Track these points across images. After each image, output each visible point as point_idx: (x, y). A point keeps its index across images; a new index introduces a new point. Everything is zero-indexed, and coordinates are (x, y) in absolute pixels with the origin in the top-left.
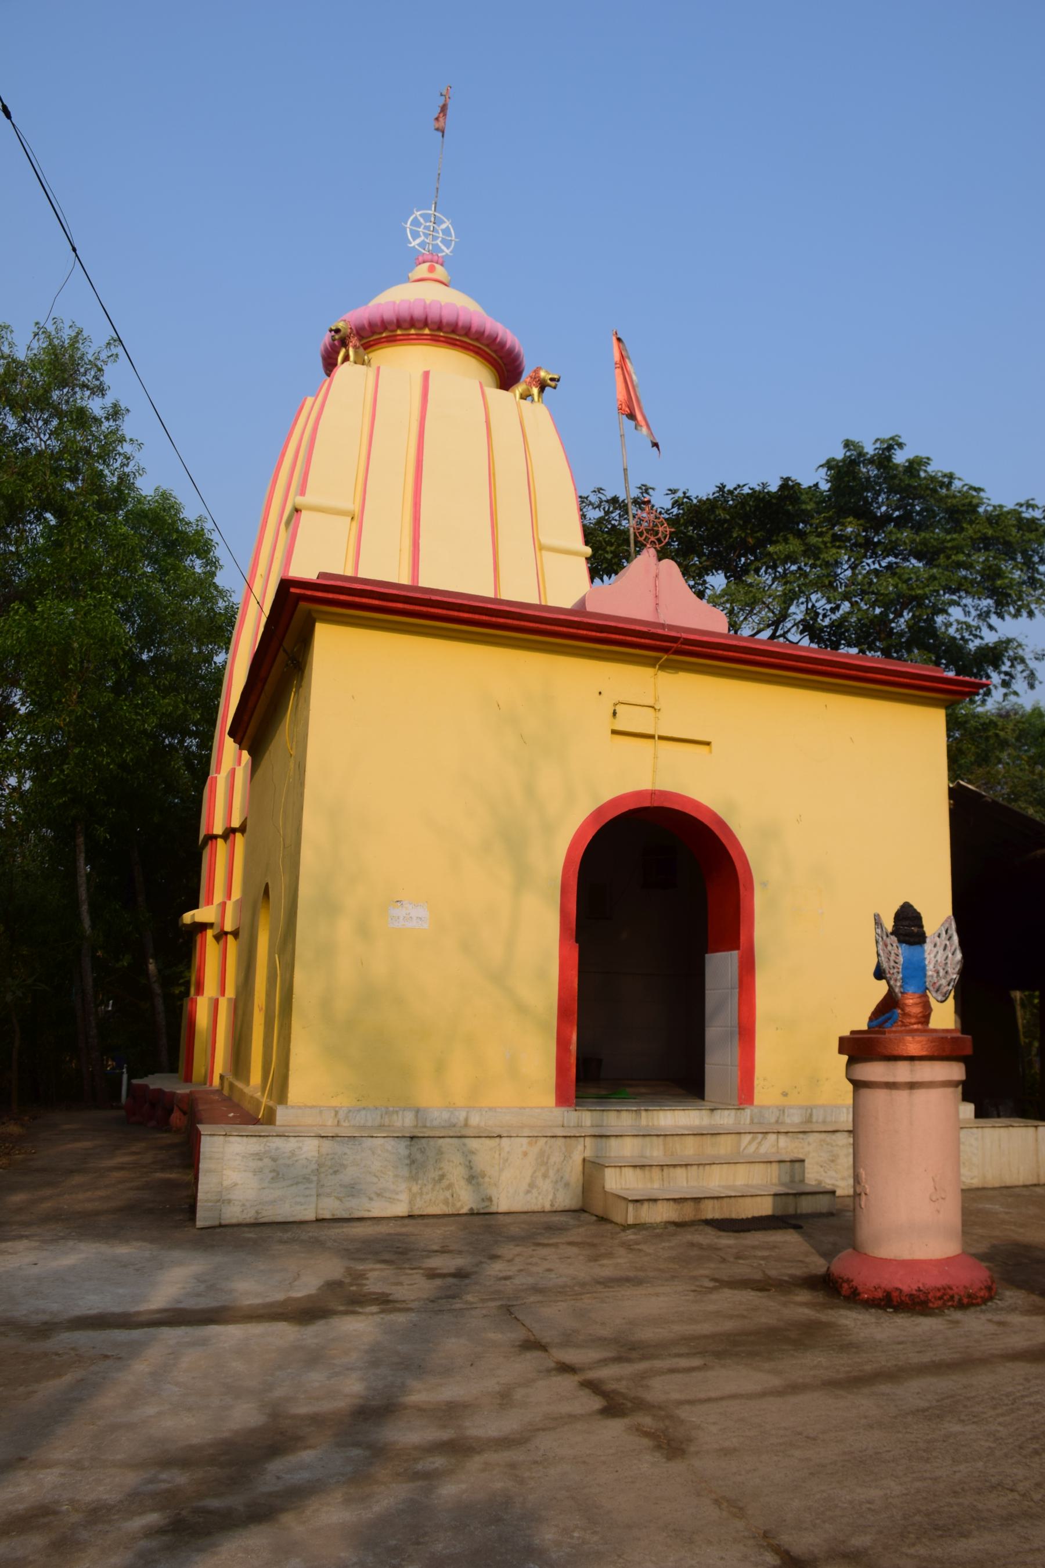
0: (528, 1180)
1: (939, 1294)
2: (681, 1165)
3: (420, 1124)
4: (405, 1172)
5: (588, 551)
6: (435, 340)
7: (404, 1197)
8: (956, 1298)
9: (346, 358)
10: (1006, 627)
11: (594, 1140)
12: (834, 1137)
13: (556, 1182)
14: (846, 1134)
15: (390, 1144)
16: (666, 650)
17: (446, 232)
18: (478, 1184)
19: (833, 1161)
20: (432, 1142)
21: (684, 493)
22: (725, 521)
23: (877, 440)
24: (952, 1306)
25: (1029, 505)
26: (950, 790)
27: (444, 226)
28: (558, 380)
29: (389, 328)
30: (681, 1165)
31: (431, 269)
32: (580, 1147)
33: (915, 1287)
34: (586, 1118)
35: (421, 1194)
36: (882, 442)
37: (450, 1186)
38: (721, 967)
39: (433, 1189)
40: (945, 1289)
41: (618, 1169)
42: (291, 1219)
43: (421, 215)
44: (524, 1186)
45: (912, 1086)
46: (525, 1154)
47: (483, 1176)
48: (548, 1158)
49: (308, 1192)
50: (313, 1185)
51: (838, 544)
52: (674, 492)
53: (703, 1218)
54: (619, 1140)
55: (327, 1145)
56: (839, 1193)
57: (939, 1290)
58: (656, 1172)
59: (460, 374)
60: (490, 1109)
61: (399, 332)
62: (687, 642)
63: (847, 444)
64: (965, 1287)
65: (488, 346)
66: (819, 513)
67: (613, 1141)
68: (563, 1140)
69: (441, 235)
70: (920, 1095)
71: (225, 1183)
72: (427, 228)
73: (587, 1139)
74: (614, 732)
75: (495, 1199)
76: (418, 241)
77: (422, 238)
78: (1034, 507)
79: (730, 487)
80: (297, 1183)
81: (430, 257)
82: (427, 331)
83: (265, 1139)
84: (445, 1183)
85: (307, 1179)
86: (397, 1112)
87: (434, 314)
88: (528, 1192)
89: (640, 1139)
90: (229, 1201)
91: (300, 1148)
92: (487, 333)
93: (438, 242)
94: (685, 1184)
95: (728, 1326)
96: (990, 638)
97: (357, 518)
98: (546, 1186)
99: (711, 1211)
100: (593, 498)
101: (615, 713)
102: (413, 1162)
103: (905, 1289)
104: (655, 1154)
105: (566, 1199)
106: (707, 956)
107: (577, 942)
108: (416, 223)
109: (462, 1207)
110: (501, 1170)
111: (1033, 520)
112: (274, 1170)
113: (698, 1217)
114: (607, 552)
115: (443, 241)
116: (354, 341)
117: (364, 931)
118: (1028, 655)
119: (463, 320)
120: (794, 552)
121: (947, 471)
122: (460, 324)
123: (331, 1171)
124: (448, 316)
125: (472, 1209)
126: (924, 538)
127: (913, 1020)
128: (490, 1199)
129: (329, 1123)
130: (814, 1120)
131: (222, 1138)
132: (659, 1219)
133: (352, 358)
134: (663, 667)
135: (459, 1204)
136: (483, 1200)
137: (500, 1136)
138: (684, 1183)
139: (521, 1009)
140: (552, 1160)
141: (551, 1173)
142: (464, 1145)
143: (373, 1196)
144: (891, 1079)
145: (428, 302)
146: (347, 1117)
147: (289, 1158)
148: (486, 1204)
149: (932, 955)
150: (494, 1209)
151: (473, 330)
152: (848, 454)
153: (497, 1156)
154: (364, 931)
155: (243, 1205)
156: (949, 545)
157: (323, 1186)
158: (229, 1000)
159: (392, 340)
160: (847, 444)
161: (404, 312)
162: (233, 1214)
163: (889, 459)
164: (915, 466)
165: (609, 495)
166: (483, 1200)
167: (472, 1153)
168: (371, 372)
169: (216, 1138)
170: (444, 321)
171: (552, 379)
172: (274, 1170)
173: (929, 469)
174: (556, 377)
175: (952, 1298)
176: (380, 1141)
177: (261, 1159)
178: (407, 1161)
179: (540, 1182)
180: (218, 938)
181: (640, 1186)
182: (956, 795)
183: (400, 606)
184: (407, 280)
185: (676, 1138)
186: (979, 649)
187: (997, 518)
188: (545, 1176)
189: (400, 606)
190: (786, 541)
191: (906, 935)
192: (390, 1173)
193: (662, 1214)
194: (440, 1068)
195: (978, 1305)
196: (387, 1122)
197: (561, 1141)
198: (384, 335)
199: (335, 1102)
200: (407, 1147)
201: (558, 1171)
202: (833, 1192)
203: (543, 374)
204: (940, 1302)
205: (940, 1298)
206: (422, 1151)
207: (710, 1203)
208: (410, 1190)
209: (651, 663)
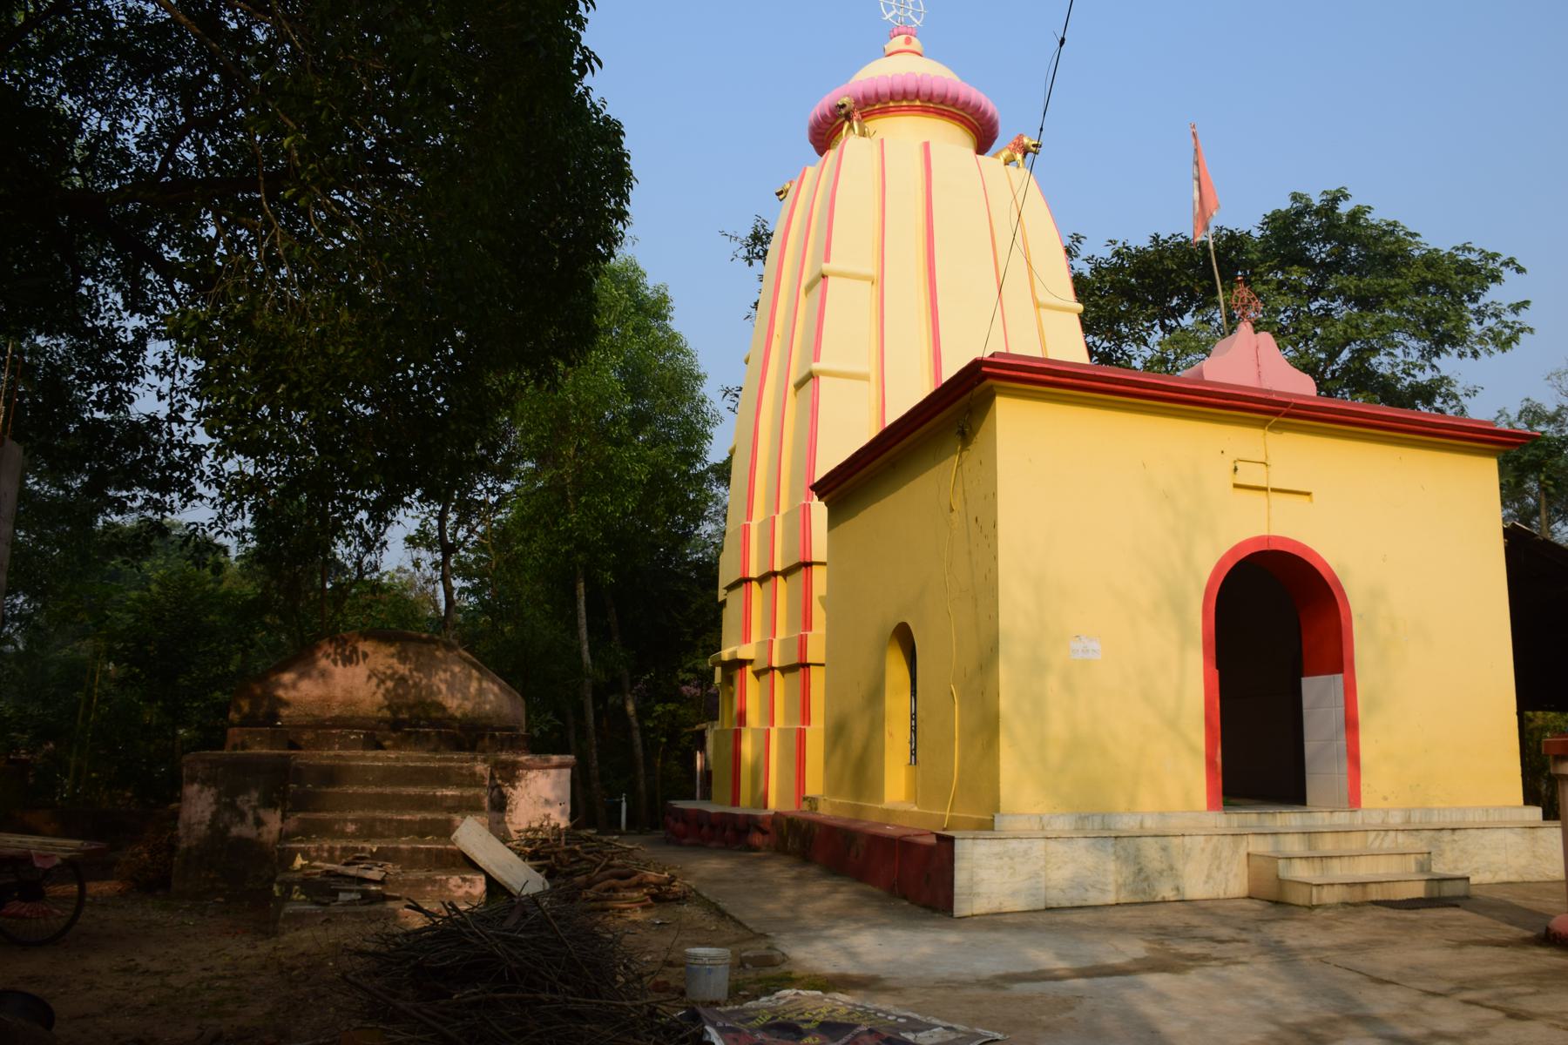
5: (1080, 307)
6: (925, 111)
10: (1449, 364)
16: (1276, 414)
22: (1172, 271)
25: (1466, 248)
26: (1505, 530)
31: (908, 41)
38: (1317, 691)
52: (1113, 242)
56: (1472, 881)
59: (950, 140)
62: (1297, 406)
63: (1295, 197)
74: (1236, 486)
78: (1470, 250)
79: (1164, 236)
84: (1143, 875)
87: (925, 88)
90: (978, 894)
96: (1423, 377)
97: (880, 282)
99: (1375, 894)
106: (1304, 680)
111: (1468, 262)
115: (914, 13)
116: (857, 115)
118: (1459, 391)
121: (1390, 220)
124: (938, 88)
134: (1272, 428)
158: (780, 730)
159: (884, 112)
160: (1295, 197)
161: (899, 87)
163: (1333, 209)
164: (1354, 216)
173: (1368, 216)
180: (758, 674)
182: (1510, 534)
183: (1069, 381)
187: (1432, 261)
189: (1069, 381)
193: (1330, 896)
197: (1229, 839)
202: (1468, 879)
203: (1026, 141)
209: (1262, 425)
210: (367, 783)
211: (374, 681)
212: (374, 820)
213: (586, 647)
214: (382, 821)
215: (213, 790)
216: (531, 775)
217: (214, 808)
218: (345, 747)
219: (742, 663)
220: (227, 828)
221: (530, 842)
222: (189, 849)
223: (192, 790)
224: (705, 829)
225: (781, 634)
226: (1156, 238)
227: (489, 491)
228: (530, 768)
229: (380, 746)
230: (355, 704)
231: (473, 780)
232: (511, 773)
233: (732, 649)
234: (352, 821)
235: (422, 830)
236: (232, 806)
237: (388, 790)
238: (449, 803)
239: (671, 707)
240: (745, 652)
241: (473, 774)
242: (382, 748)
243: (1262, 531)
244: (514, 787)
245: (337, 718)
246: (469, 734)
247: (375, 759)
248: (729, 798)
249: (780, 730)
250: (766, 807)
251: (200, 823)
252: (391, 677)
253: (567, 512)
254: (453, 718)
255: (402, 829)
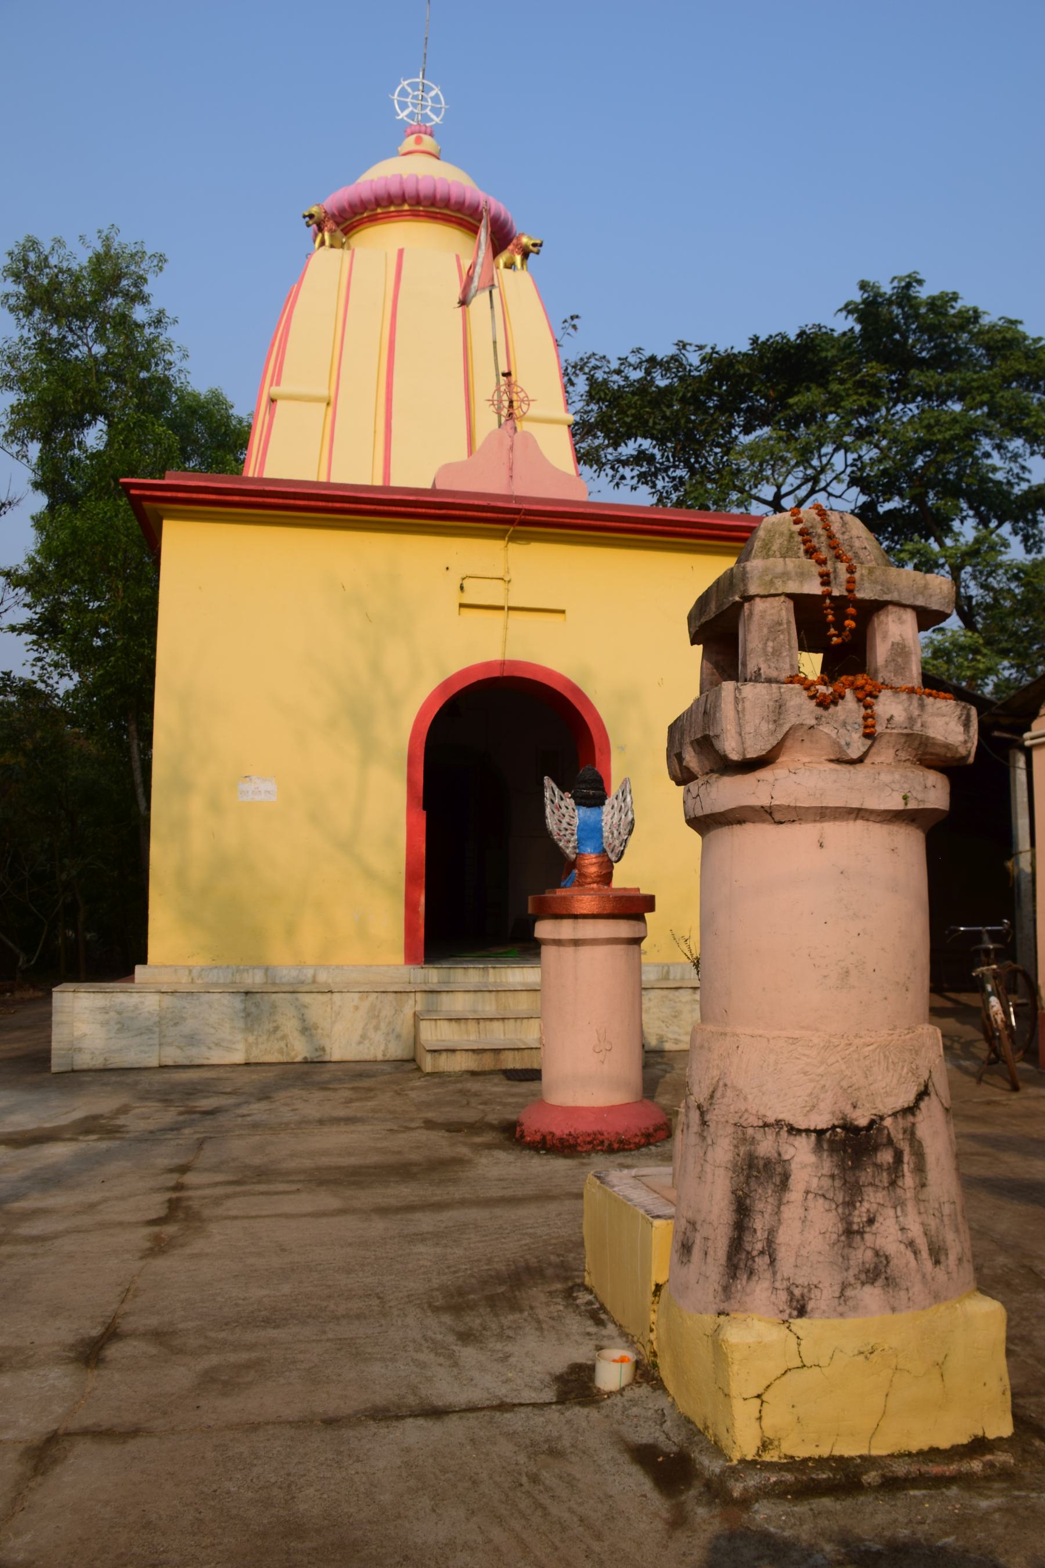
0: (360, 1032)
1: (589, 1139)
2: (498, 1019)
3: (270, 981)
4: (241, 1024)
6: (415, 215)
7: (241, 1046)
8: (606, 1143)
9: (323, 243)
11: (424, 995)
12: (677, 993)
13: (388, 1034)
14: (690, 990)
15: (226, 999)
16: (511, 522)
17: (436, 99)
18: (311, 1035)
19: (675, 1017)
20: (266, 997)
21: (713, 348)
22: (745, 375)
23: (894, 278)
24: (602, 1150)
27: (432, 94)
28: (541, 245)
29: (384, 203)
30: (498, 1019)
31: (418, 141)
32: (411, 1002)
33: (567, 1132)
34: (433, 975)
35: (257, 1044)
36: (901, 279)
37: (284, 1037)
39: (268, 1040)
40: (595, 1134)
41: (433, 1022)
42: (137, 1066)
43: (408, 85)
44: (356, 1037)
45: (576, 943)
46: (357, 1008)
47: (316, 1029)
48: (380, 1012)
49: (151, 1042)
50: (156, 1036)
51: (860, 391)
53: (504, 1068)
54: (450, 995)
55: (168, 1000)
57: (589, 1135)
58: (472, 1026)
60: (337, 967)
61: (379, 211)
63: (863, 286)
64: (617, 1133)
65: (471, 215)
66: (842, 360)
67: (444, 996)
68: (394, 995)
69: (430, 103)
70: (585, 951)
71: (76, 1034)
72: (415, 97)
73: (418, 994)
74: (462, 606)
75: (328, 1049)
76: (406, 112)
77: (411, 109)
80: (141, 1034)
81: (417, 128)
82: (406, 207)
83: (111, 995)
84: (279, 1034)
85: (149, 1030)
86: (247, 970)
87: (410, 189)
88: (360, 1043)
89: (471, 995)
90: (80, 1050)
91: (142, 1003)
92: (467, 204)
93: (428, 111)
94: (502, 1037)
95: (352, 1161)
98: (378, 1037)
100: (633, 359)
101: (462, 588)
102: (248, 1015)
103: (558, 1133)
104: (487, 1008)
105: (397, 1051)
107: (424, 809)
108: (404, 93)
109: (296, 1056)
110: (333, 1023)
112: (119, 1023)
113: (498, 1067)
114: (628, 416)
115: (433, 110)
117: (215, 806)
119: (441, 191)
120: (813, 401)
122: (438, 196)
123: (172, 1023)
124: (425, 189)
125: (305, 1058)
126: (950, 379)
127: (589, 880)
128: (323, 1049)
129: (184, 981)
130: (671, 977)
131: (71, 994)
132: (457, 1068)
133: (327, 243)
134: (513, 539)
135: (293, 1054)
136: (316, 1050)
137: (331, 992)
138: (498, 1035)
139: (370, 874)
140: (383, 1013)
141: (383, 1026)
142: (297, 999)
143: (211, 1045)
144: (557, 937)
145: (405, 177)
146: (200, 976)
147: (133, 1011)
148: (318, 1054)
149: (610, 817)
150: (327, 1058)
151: (453, 201)
152: (866, 295)
153: (329, 1009)
154: (215, 806)
155: (93, 1053)
156: (975, 384)
157: (165, 1036)
159: (374, 219)
160: (863, 286)
161: (381, 190)
162: (83, 1061)
165: (647, 354)
166: (316, 1050)
167: (305, 1007)
168: (347, 254)
169: (66, 994)
170: (422, 195)
171: (534, 245)
172: (119, 1023)
174: (538, 242)
175: (602, 1142)
176: (217, 996)
177: (107, 1013)
178: (243, 1014)
179: (371, 1033)
181: (456, 1038)
183: (237, 498)
184: (394, 153)
185: (509, 994)
186: (1026, 493)
188: (377, 1028)
190: (808, 389)
191: (583, 797)
192: (227, 1025)
194: (291, 930)
195: (630, 1150)
196: (238, 978)
197: (391, 996)
198: (365, 215)
199: (191, 962)
200: (242, 1001)
201: (390, 1023)
204: (590, 1147)
205: (589, 1143)
206: (257, 1005)
207: (510, 1054)
208: (246, 1040)
209: (500, 536)
226: (755, 340)
243: (494, 655)
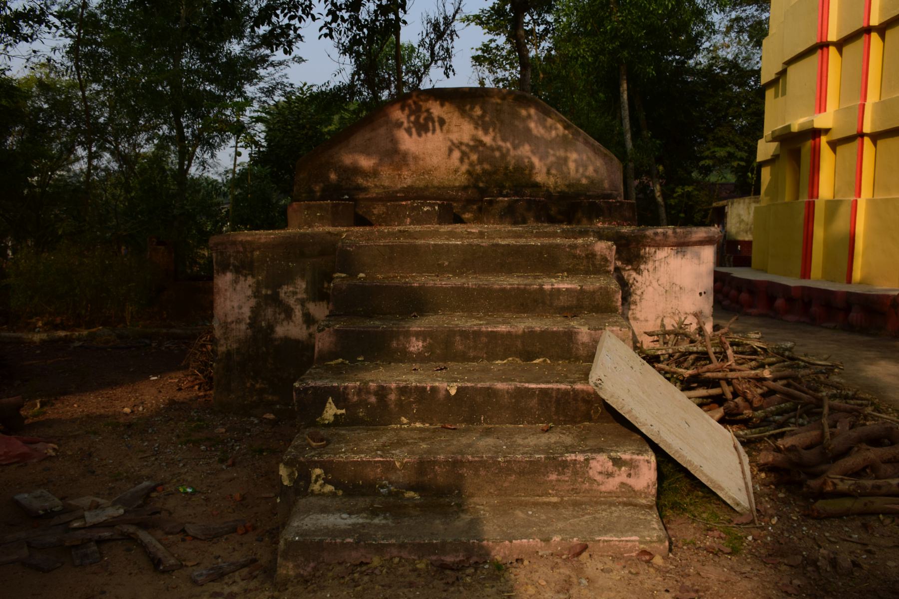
210: (440, 270)
211: (456, 154)
212: (451, 333)
213: (629, 136)
214: (464, 334)
215: (250, 280)
216: (662, 254)
217: (253, 302)
218: (416, 221)
219: (815, 133)
220: (271, 328)
221: (681, 359)
222: (228, 354)
223: (224, 280)
224: (779, 302)
225: (873, 97)
227: (536, 22)
228: (659, 246)
229: (458, 220)
230: (428, 172)
231: (591, 265)
232: (631, 253)
233: (802, 120)
234: (418, 335)
235: (527, 348)
236: (275, 300)
237: (471, 282)
238: (563, 301)
239: (690, 189)
240: (821, 121)
241: (591, 256)
242: (461, 221)
244: (638, 271)
245: (410, 188)
246: (570, 206)
247: (452, 235)
248: (798, 267)
249: (872, 203)
250: (849, 280)
251: (239, 321)
252: (474, 149)
253: (611, 14)
254: (549, 195)
255: (498, 347)
